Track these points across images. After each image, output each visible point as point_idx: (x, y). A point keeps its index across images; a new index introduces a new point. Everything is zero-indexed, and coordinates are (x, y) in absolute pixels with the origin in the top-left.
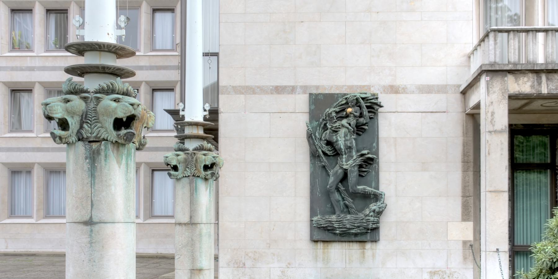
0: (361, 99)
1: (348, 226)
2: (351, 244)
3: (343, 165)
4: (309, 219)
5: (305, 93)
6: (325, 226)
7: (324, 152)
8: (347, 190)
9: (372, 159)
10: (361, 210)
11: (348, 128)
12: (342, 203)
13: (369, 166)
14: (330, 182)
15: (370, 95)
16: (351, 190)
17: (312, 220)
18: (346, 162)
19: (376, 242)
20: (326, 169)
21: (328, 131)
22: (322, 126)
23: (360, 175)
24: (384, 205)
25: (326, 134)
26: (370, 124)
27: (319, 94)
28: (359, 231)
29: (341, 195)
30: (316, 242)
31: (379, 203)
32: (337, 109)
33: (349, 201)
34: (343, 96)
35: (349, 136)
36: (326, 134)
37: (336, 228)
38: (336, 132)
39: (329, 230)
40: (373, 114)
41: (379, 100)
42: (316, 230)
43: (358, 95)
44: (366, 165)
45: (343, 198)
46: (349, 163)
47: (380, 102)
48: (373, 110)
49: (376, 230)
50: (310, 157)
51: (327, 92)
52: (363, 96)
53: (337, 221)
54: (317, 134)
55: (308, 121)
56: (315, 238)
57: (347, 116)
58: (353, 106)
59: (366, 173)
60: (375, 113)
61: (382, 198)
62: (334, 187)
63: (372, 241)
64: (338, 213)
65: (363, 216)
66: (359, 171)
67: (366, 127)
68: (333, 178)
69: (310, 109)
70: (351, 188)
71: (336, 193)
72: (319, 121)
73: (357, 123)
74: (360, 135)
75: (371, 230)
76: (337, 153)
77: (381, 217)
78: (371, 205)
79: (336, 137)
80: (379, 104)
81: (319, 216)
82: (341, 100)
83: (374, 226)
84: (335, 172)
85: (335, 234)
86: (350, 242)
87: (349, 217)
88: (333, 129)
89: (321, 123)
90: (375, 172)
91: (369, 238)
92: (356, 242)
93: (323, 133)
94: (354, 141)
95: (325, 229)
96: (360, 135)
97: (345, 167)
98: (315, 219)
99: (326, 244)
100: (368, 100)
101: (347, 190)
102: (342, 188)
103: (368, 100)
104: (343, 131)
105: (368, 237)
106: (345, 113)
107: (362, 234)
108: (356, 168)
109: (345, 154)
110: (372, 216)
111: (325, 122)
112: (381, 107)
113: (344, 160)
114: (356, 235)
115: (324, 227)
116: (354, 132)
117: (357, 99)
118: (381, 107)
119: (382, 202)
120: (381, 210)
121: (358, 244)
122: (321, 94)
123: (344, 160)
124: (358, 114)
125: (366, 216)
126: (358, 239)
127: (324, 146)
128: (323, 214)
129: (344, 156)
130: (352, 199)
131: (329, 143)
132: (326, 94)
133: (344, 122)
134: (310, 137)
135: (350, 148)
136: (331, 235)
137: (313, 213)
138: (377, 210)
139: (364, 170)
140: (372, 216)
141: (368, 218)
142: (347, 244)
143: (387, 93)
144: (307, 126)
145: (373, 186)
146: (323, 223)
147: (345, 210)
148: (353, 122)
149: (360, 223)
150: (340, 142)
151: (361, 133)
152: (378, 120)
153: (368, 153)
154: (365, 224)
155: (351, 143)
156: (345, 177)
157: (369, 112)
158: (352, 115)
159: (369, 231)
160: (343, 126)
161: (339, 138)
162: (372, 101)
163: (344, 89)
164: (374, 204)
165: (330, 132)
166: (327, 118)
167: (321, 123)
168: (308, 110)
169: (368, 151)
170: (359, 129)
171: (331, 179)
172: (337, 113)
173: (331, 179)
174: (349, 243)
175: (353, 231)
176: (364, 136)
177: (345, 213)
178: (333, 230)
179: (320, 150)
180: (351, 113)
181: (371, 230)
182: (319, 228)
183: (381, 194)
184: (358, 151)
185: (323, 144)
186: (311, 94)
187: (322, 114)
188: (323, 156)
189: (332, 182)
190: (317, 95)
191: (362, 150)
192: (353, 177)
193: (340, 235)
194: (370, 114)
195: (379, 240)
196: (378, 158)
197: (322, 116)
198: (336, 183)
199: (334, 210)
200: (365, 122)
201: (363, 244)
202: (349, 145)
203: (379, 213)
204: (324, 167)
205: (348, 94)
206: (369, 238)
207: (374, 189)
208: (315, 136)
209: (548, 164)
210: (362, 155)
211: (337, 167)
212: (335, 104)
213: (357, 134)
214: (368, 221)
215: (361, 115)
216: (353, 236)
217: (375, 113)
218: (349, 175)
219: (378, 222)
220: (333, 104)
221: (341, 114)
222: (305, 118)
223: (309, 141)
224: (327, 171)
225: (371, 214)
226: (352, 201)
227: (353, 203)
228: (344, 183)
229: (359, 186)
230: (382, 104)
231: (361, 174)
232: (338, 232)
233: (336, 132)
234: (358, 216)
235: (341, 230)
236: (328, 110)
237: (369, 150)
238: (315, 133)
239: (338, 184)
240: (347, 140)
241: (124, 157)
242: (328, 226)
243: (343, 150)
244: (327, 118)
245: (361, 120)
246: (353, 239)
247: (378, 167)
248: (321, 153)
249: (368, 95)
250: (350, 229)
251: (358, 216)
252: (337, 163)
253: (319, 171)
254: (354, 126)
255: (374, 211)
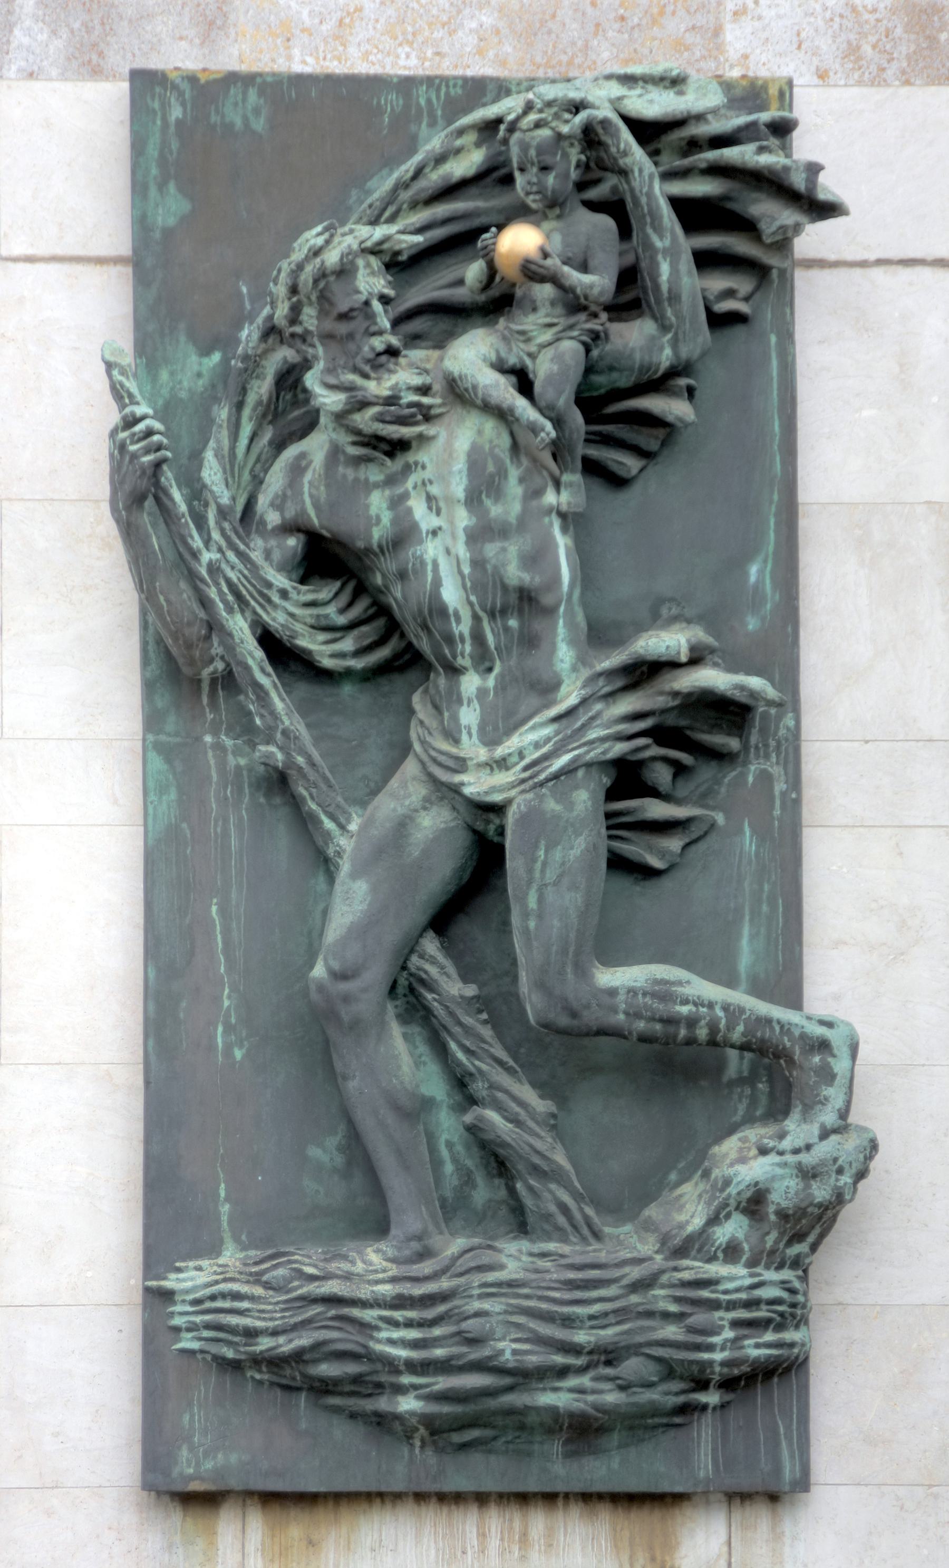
0: (626, 136)
1: (507, 1349)
2: (538, 1521)
3: (461, 765)
4: (136, 1281)
5: (96, 72)
6: (286, 1345)
7: (277, 639)
8: (498, 1006)
9: (732, 712)
10: (633, 1197)
11: (502, 415)
12: (448, 1126)
13: (706, 772)
14: (335, 929)
15: (714, 98)
16: (533, 1004)
17: (167, 1296)
18: (490, 738)
19: (774, 1498)
20: (295, 803)
21: (316, 446)
22: (262, 388)
23: (619, 864)
24: (845, 1148)
25: (298, 468)
26: (712, 379)
27: (232, 78)
28: (612, 1397)
29: (441, 1050)
30: (200, 1501)
31: (797, 1130)
32: (403, 234)
33: (518, 1109)
34: (455, 108)
35: (514, 489)
36: (298, 468)
37: (391, 1365)
38: (397, 447)
39: (323, 1389)
40: (743, 284)
41: (805, 147)
42: (205, 1386)
43: (603, 99)
44: (680, 770)
45: (460, 1082)
46: (517, 744)
47: (814, 169)
48: (739, 245)
49: (774, 1379)
50: (149, 687)
51: (302, 62)
52: (653, 105)
53: (400, 1302)
54: (212, 473)
55: (124, 342)
56: (193, 1467)
57: (497, 303)
58: (551, 207)
59: (674, 844)
60: (759, 271)
61: (828, 1076)
62: (376, 975)
63: (739, 1497)
64: (409, 1218)
65: (647, 1246)
66: (616, 824)
67: (673, 408)
68: (361, 887)
69: (141, 225)
70: (541, 985)
71: (396, 1030)
72: (226, 342)
73: (589, 370)
74: (617, 481)
75: (728, 1384)
76: (403, 655)
77: (820, 1263)
78: (730, 1146)
79: (397, 502)
80: (799, 181)
81: (230, 1256)
82: (435, 143)
83: (755, 1349)
84: (387, 835)
85: (382, 1423)
86: (523, 1499)
87: (514, 1257)
88: (365, 420)
89: (252, 364)
90: (762, 834)
91: (704, 1461)
92: (589, 1498)
93: (265, 463)
94: (562, 542)
95: (288, 1377)
96: (617, 481)
97: (476, 785)
98: (191, 1278)
99: (296, 1526)
100: (694, 145)
101: (498, 1006)
102: (450, 986)
103: (694, 145)
104: (456, 442)
105: (704, 1450)
106: (474, 271)
107: (640, 1424)
108: (585, 798)
109: (483, 661)
110: (731, 1252)
111: (284, 354)
112: (825, 210)
113: (469, 716)
114: (583, 1431)
115: (275, 1362)
116: (558, 450)
117: (591, 137)
118: (825, 210)
119: (829, 1117)
120: (821, 1192)
121: (605, 1517)
122: (247, 80)
123: (469, 716)
124: (598, 282)
125: (681, 1251)
126: (606, 1469)
127: (280, 580)
128: (268, 1233)
129: (470, 683)
130: (543, 1088)
131: (324, 557)
132: (299, 80)
133: (472, 355)
134: (143, 492)
135: (527, 602)
136: (341, 1432)
137: (170, 1217)
138: (785, 1192)
139: (656, 810)
140: (731, 1252)
141: (694, 1268)
142: (496, 1520)
143: (878, 80)
144: (119, 394)
145: (745, 960)
146: (268, 1320)
147: (484, 1192)
148: (556, 358)
149: (622, 1314)
150: (431, 550)
151: (629, 463)
152: (787, 336)
153: (696, 659)
154: (672, 1331)
155: (540, 556)
156: (478, 877)
157: (706, 261)
158: (545, 291)
159: (712, 1398)
160: (459, 393)
161: (418, 508)
162: (731, 154)
163: (466, 40)
164: (753, 1134)
165: (335, 452)
166: (310, 318)
167: (252, 364)
168: (116, 238)
169: (699, 634)
170: (614, 426)
171: (351, 903)
172: (400, 266)
173: (351, 903)
174: (515, 1517)
175: (556, 1398)
176: (660, 489)
177: (478, 1220)
178: (361, 1386)
179: (239, 626)
180: (532, 272)
181: (728, 1384)
182: (235, 1366)
183: (824, 1046)
184: (599, 635)
185: (270, 561)
186: (146, 83)
187: (261, 278)
188: (266, 677)
189: (360, 931)
190: (209, 92)
191: (640, 628)
192: (554, 875)
193: (436, 1430)
194: (718, 282)
195: (803, 1483)
196: (790, 699)
197: (261, 295)
198: (392, 935)
199: (377, 1190)
200: (666, 357)
201: (641, 1521)
202: (515, 574)
203: (804, 1226)
204: (278, 782)
205: (502, 89)
206: (704, 1461)
207: (758, 990)
208: (197, 492)
209: (745, 1077)
210: (642, 673)
211: (406, 789)
212: (382, 185)
213: (592, 468)
214: (697, 1297)
215: (631, 294)
216: (556, 1447)
217: (759, 271)
218: (514, 863)
219: (792, 1313)
220: (360, 181)
221: (447, 272)
222: (90, 315)
223: (131, 534)
224: (304, 823)
225: (724, 1233)
226: (541, 1106)
227: (553, 1125)
228: (467, 927)
229: (611, 960)
230: (830, 185)
231: (637, 848)
232: (408, 1404)
233: (397, 447)
234: (598, 1252)
235: (442, 1383)
236: (313, 237)
237: (707, 619)
238: (196, 457)
239: (411, 947)
240: (501, 531)
241: (674, 989)
242: (319, 1351)
243: (464, 628)
244: (310, 318)
245: (634, 338)
246: (556, 1467)
247: (795, 782)
248: (253, 654)
249: (699, 98)
250: (524, 1377)
251: (598, 1252)
252: (405, 749)
253: (235, 821)
254: (565, 400)
255: (754, 1203)
